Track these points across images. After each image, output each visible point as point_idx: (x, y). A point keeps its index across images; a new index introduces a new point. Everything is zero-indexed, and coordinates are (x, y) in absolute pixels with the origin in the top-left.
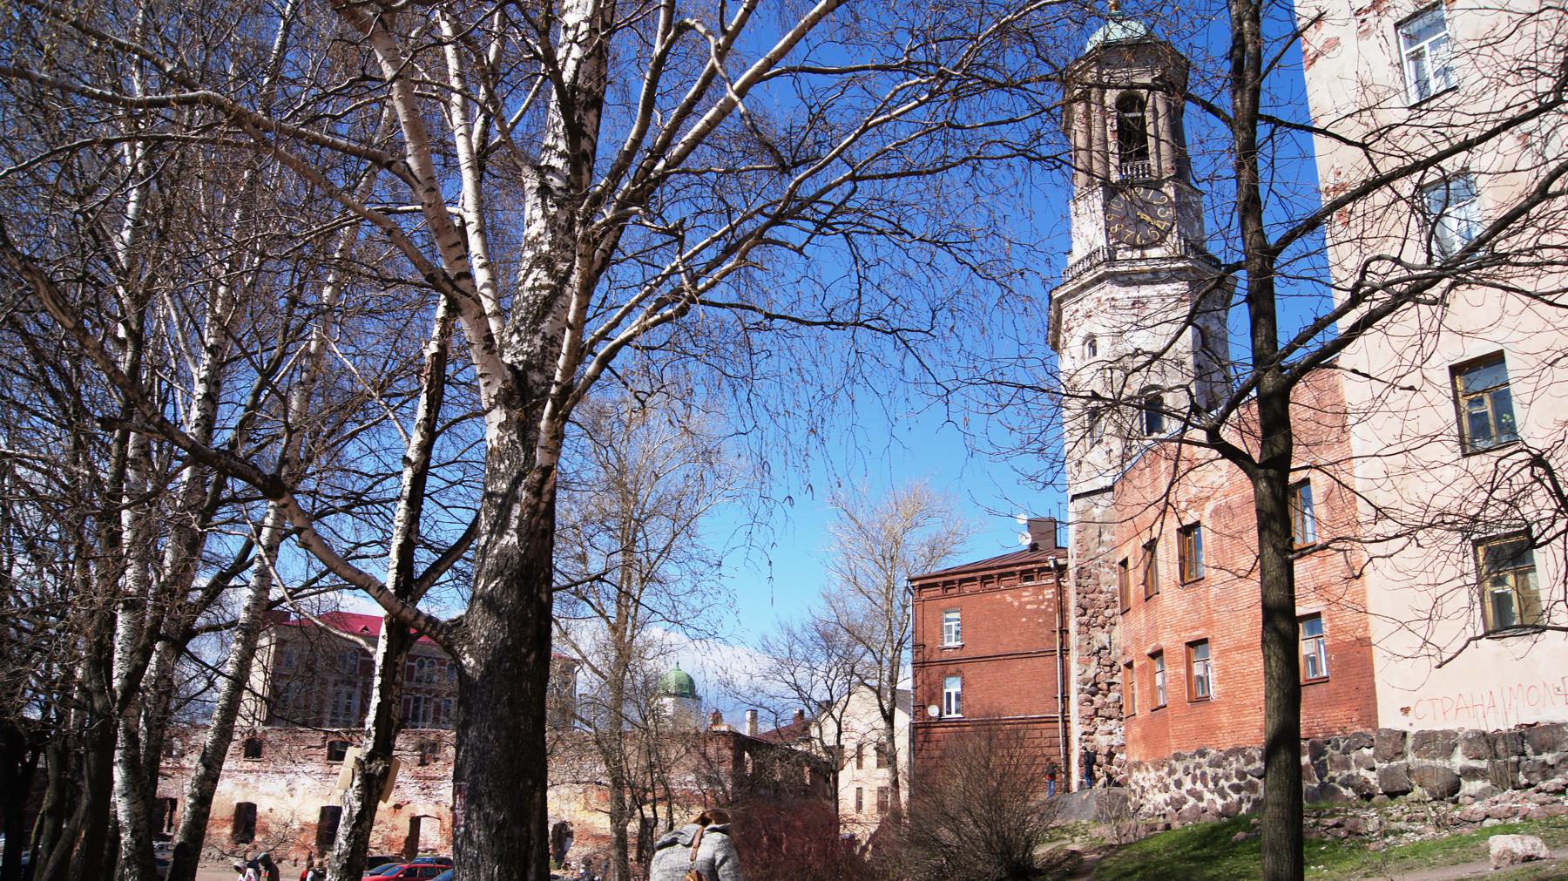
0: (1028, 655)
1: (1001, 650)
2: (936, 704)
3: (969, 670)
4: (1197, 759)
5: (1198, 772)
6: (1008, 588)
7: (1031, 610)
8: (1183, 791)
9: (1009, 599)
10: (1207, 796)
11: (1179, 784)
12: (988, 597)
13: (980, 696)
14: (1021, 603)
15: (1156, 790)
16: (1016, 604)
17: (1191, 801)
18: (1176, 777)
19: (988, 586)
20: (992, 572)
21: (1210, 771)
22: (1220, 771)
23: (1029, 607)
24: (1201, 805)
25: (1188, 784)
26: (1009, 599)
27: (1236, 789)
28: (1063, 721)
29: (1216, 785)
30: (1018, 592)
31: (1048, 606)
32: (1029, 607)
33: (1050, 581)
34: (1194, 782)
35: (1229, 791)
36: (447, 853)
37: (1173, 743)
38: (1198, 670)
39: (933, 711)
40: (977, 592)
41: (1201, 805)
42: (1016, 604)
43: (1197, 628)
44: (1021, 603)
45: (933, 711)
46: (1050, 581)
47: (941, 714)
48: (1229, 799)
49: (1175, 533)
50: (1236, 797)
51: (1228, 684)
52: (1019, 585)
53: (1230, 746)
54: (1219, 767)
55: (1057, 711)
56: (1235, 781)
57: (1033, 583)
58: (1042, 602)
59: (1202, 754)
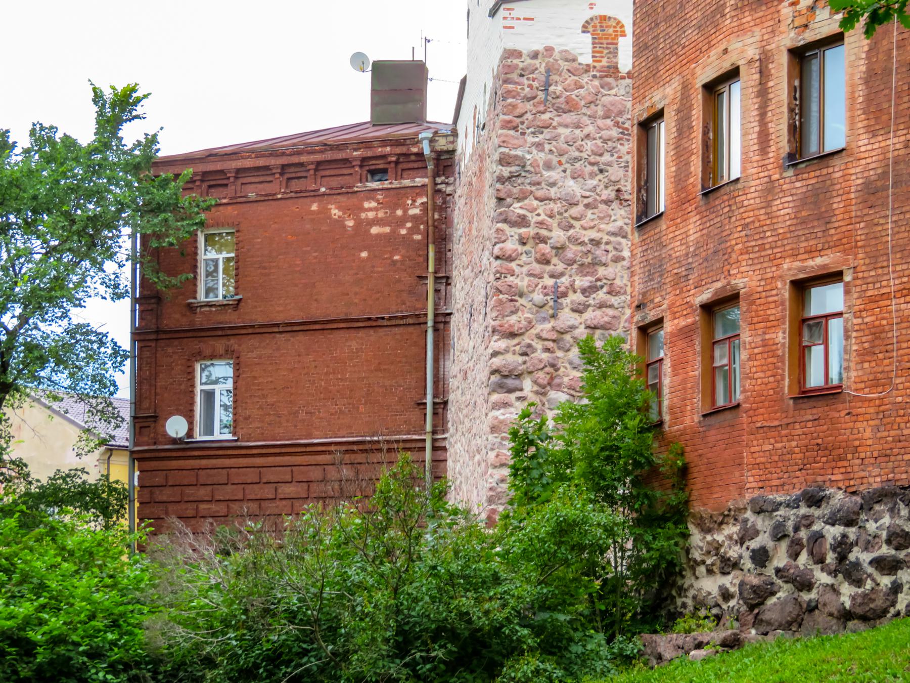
0: (372, 323)
1: (318, 312)
2: (179, 412)
3: (253, 349)
4: (803, 510)
5: (803, 534)
6: (334, 193)
7: (379, 236)
8: (770, 571)
9: (335, 212)
10: (822, 578)
11: (761, 557)
12: (294, 207)
13: (270, 400)
14: (359, 223)
15: (702, 569)
16: (350, 223)
17: (784, 592)
18: (754, 544)
19: (296, 185)
20: (304, 159)
21: (833, 532)
22: (852, 532)
23: (375, 230)
24: (806, 597)
25: (780, 559)
26: (335, 212)
27: (880, 564)
28: (435, 449)
29: (842, 558)
30: (354, 200)
31: (412, 231)
32: (375, 230)
33: (419, 181)
34: (795, 556)
35: (870, 570)
36: (802, 529)
37: (751, 481)
38: (721, 360)
39: (176, 427)
40: (269, 198)
41: (806, 597)
42: (350, 223)
43: (820, 252)
44: (359, 223)
45: (176, 427)
46: (419, 181)
47: (190, 433)
48: (869, 585)
49: (701, 89)
50: (886, 581)
51: (879, 362)
52: (358, 187)
53: (876, 483)
54: (850, 523)
55: (422, 430)
56: (885, 550)
57: (386, 185)
58: (401, 222)
59: (815, 500)
